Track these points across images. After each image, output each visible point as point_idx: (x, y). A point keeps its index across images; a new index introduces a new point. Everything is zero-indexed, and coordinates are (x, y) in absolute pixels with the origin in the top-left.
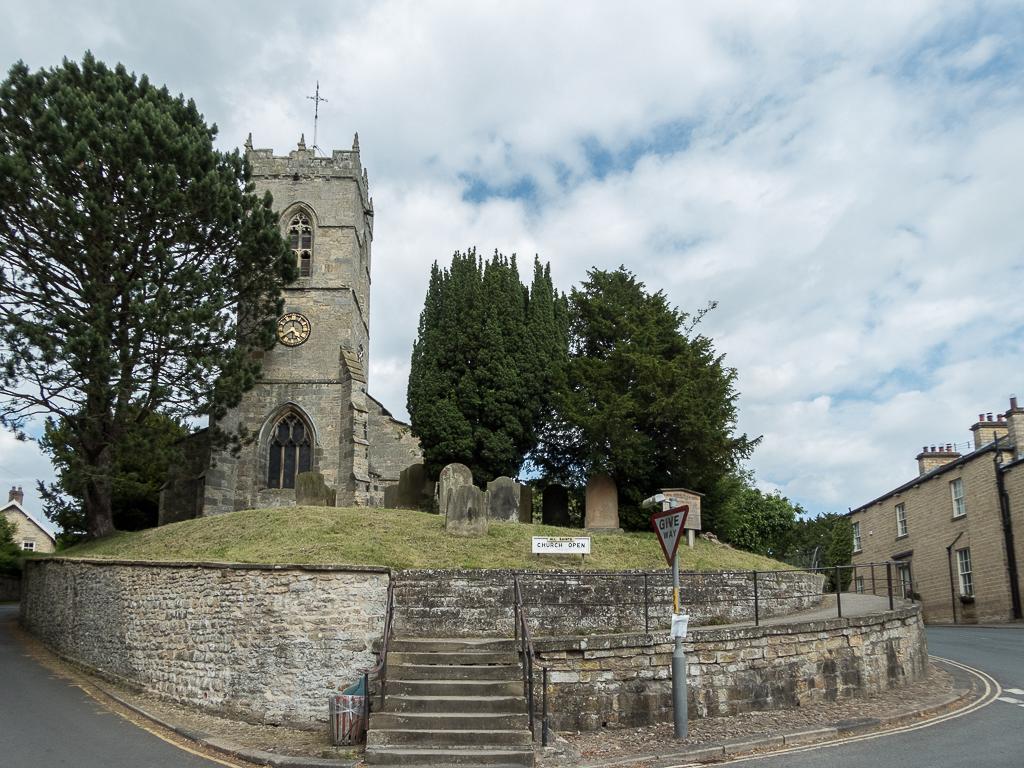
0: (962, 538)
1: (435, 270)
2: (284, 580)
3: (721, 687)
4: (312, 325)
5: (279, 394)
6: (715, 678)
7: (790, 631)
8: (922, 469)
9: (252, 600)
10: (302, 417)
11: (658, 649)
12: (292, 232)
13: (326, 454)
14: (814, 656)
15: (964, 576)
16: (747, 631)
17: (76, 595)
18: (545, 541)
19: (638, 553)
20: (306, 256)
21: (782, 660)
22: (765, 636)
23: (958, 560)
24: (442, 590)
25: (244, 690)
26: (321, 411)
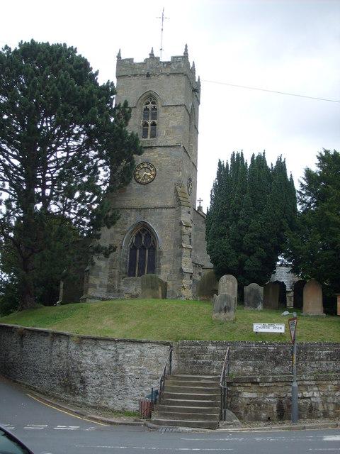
1: (220, 163)
12: (145, 110)
18: (260, 326)
24: (204, 351)
26: (162, 226)
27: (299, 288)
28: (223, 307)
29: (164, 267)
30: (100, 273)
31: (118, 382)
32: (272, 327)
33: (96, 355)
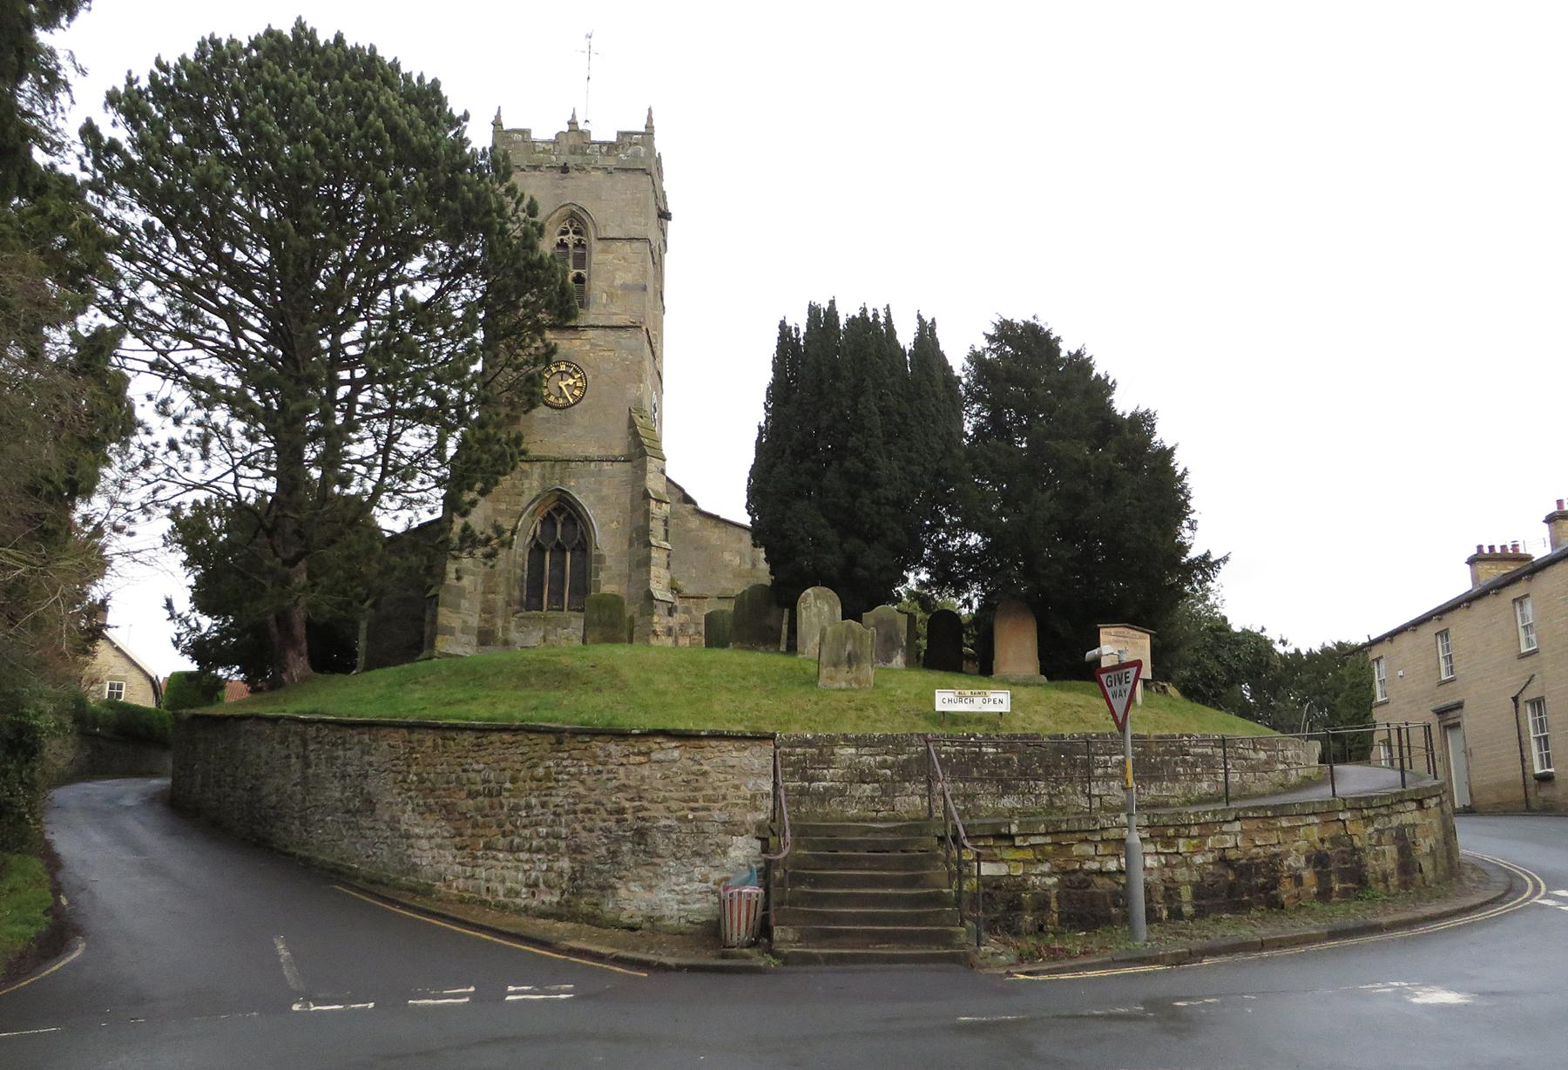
0: (1534, 683)
1: (783, 325)
2: (643, 749)
3: (1183, 884)
4: (589, 377)
5: (543, 477)
6: (1178, 871)
8: (1475, 579)
9: (600, 772)
10: (575, 510)
11: (1105, 835)
13: (609, 562)
14: (1302, 844)
15: (1539, 739)
16: (1214, 813)
18: (951, 696)
19: (1070, 712)
20: (579, 279)
21: (1261, 851)
22: (1237, 819)
23: (1529, 718)
25: (589, 886)
31: (627, 847)
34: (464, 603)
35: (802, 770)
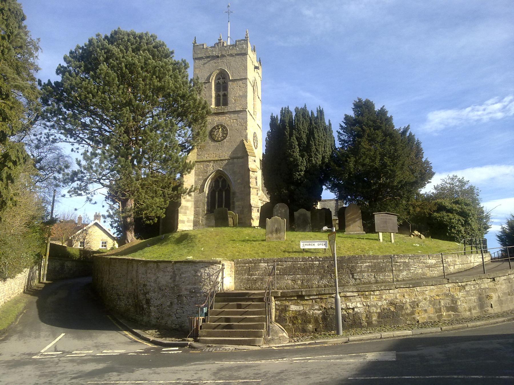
7: (411, 286)
17: (110, 274)
27: (341, 213)
28: (274, 229)
29: (237, 204)
30: (188, 211)
32: (314, 243)
33: (158, 277)
34: (188, 212)
35: (249, 271)
